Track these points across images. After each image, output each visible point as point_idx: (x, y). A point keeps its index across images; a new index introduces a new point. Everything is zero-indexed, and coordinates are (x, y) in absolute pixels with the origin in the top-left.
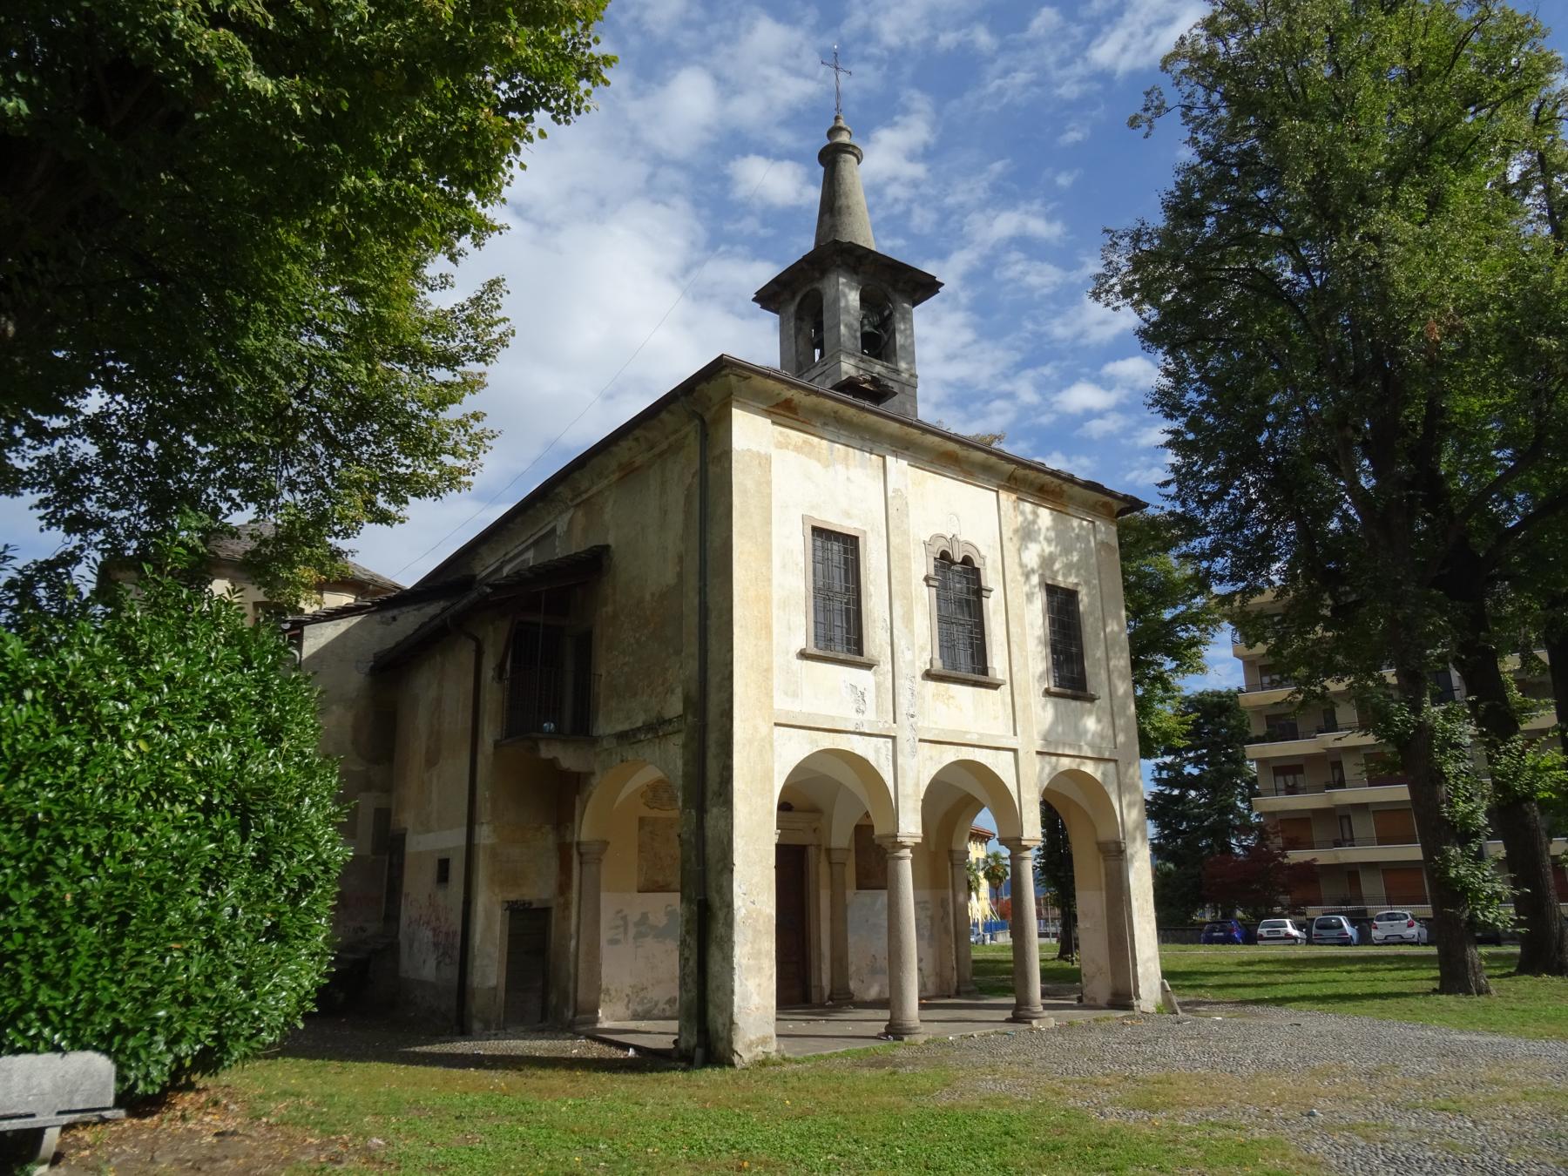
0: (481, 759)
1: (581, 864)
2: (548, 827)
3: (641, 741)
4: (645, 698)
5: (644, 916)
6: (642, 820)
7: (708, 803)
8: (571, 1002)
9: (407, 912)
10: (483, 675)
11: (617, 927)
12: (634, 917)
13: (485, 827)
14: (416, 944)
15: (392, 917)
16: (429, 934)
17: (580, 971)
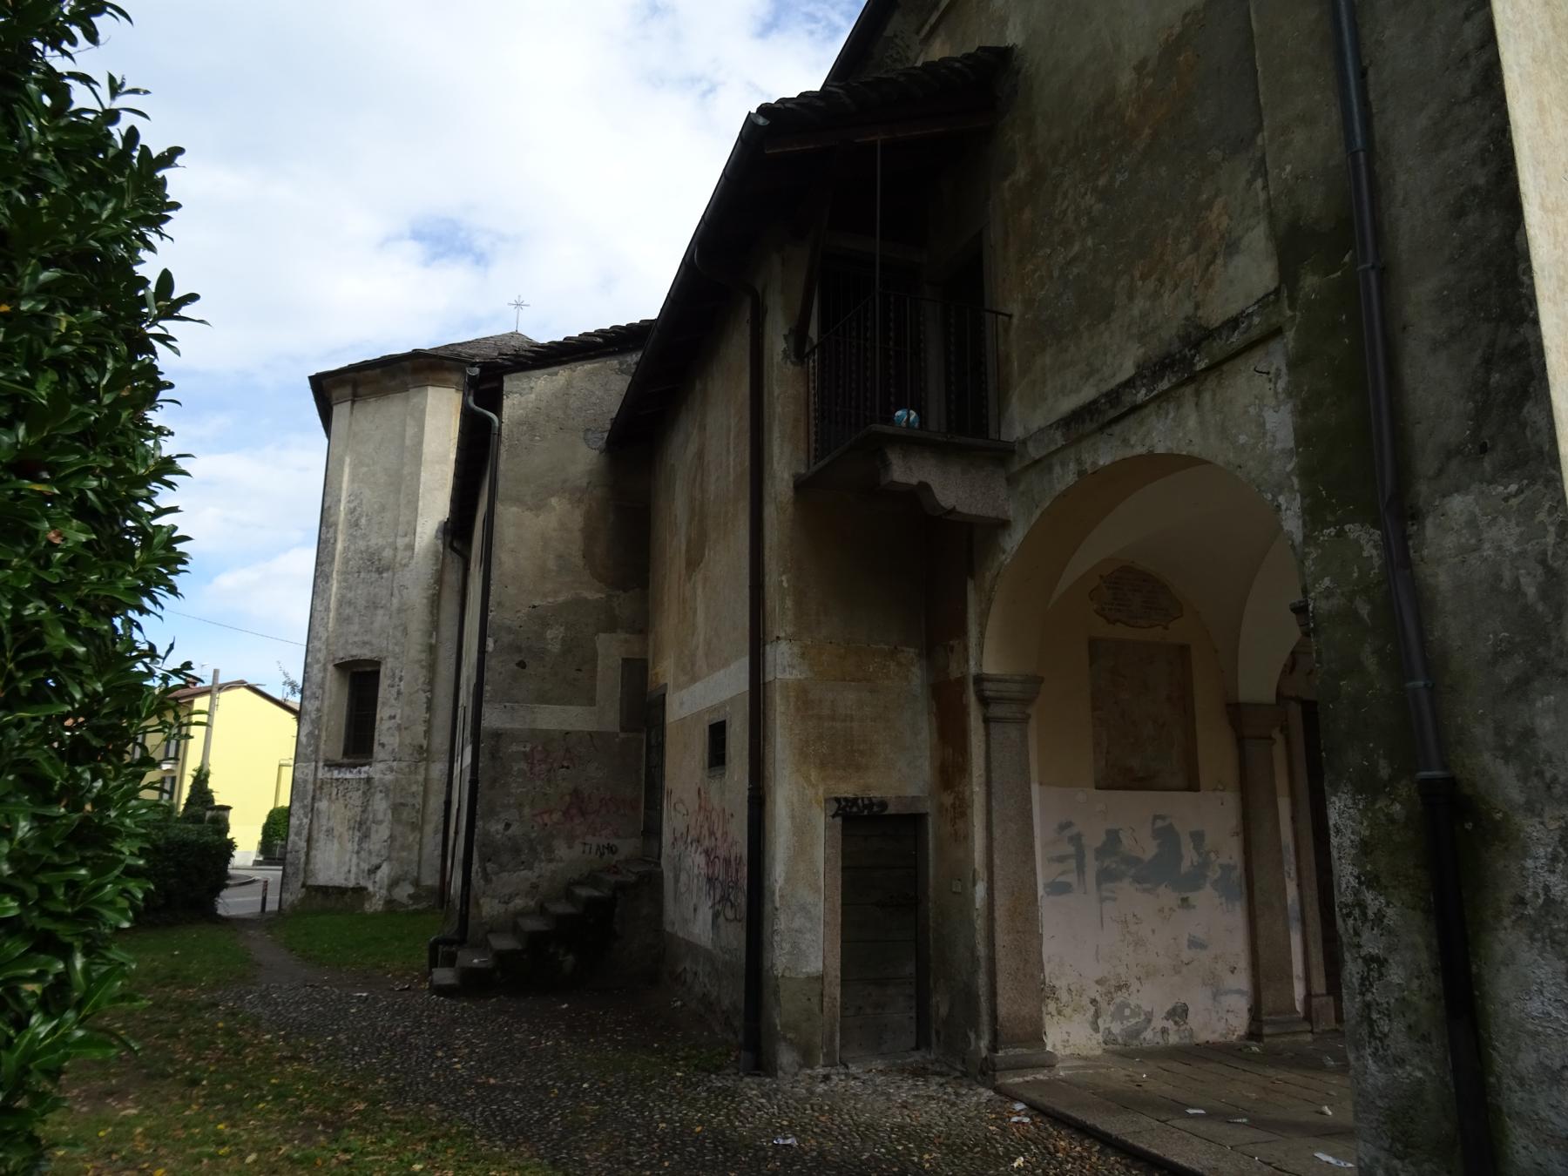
0: (770, 512)
1: (987, 721)
2: (911, 652)
3: (1136, 408)
4: (1139, 305)
5: (1113, 837)
6: (1093, 644)
7: (1423, 488)
8: (985, 1018)
9: (673, 821)
10: (767, 353)
11: (1061, 859)
12: (1094, 838)
13: (783, 646)
14: (683, 877)
15: (652, 831)
16: (700, 859)
17: (1000, 953)
